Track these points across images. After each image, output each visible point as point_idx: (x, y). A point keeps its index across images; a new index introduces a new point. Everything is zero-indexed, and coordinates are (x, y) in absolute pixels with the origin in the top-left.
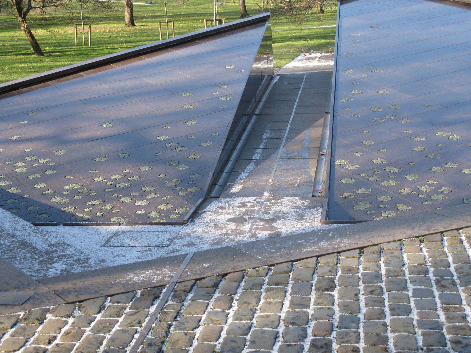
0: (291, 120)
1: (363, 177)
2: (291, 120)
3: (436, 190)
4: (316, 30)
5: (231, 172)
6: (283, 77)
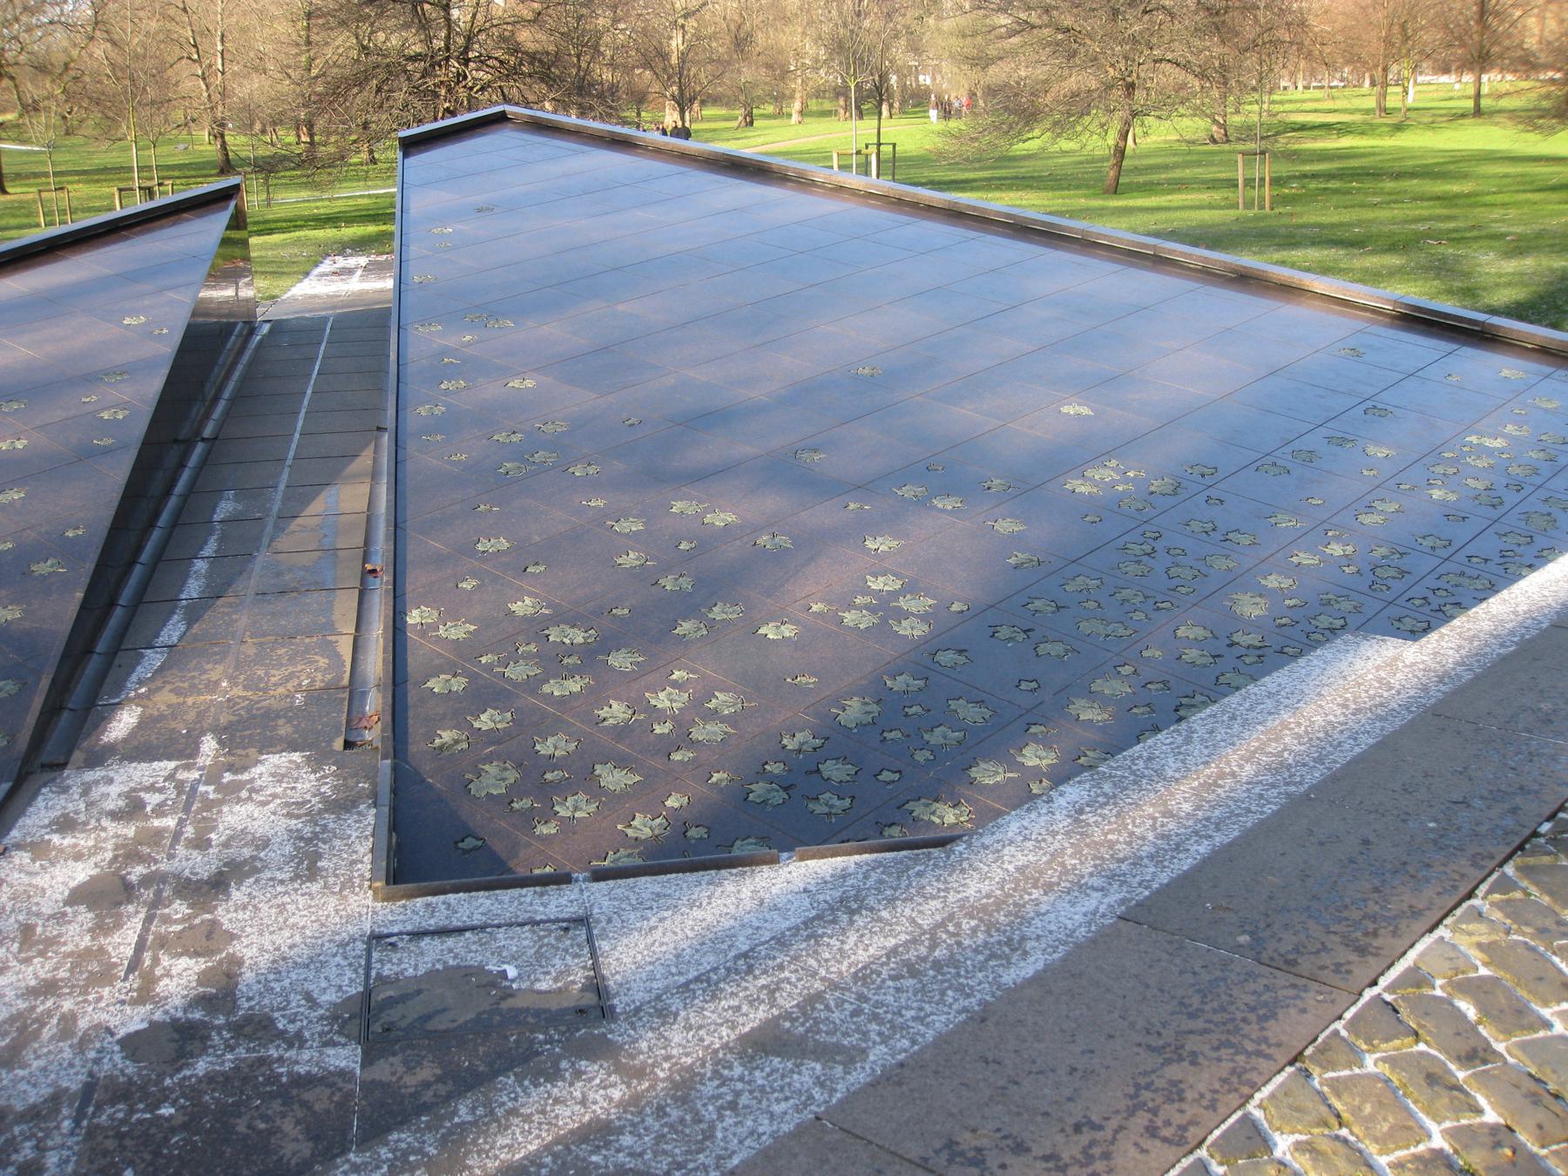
0: (291, 454)
1: (489, 668)
2: (291, 454)
3: (699, 708)
6: (278, 327)
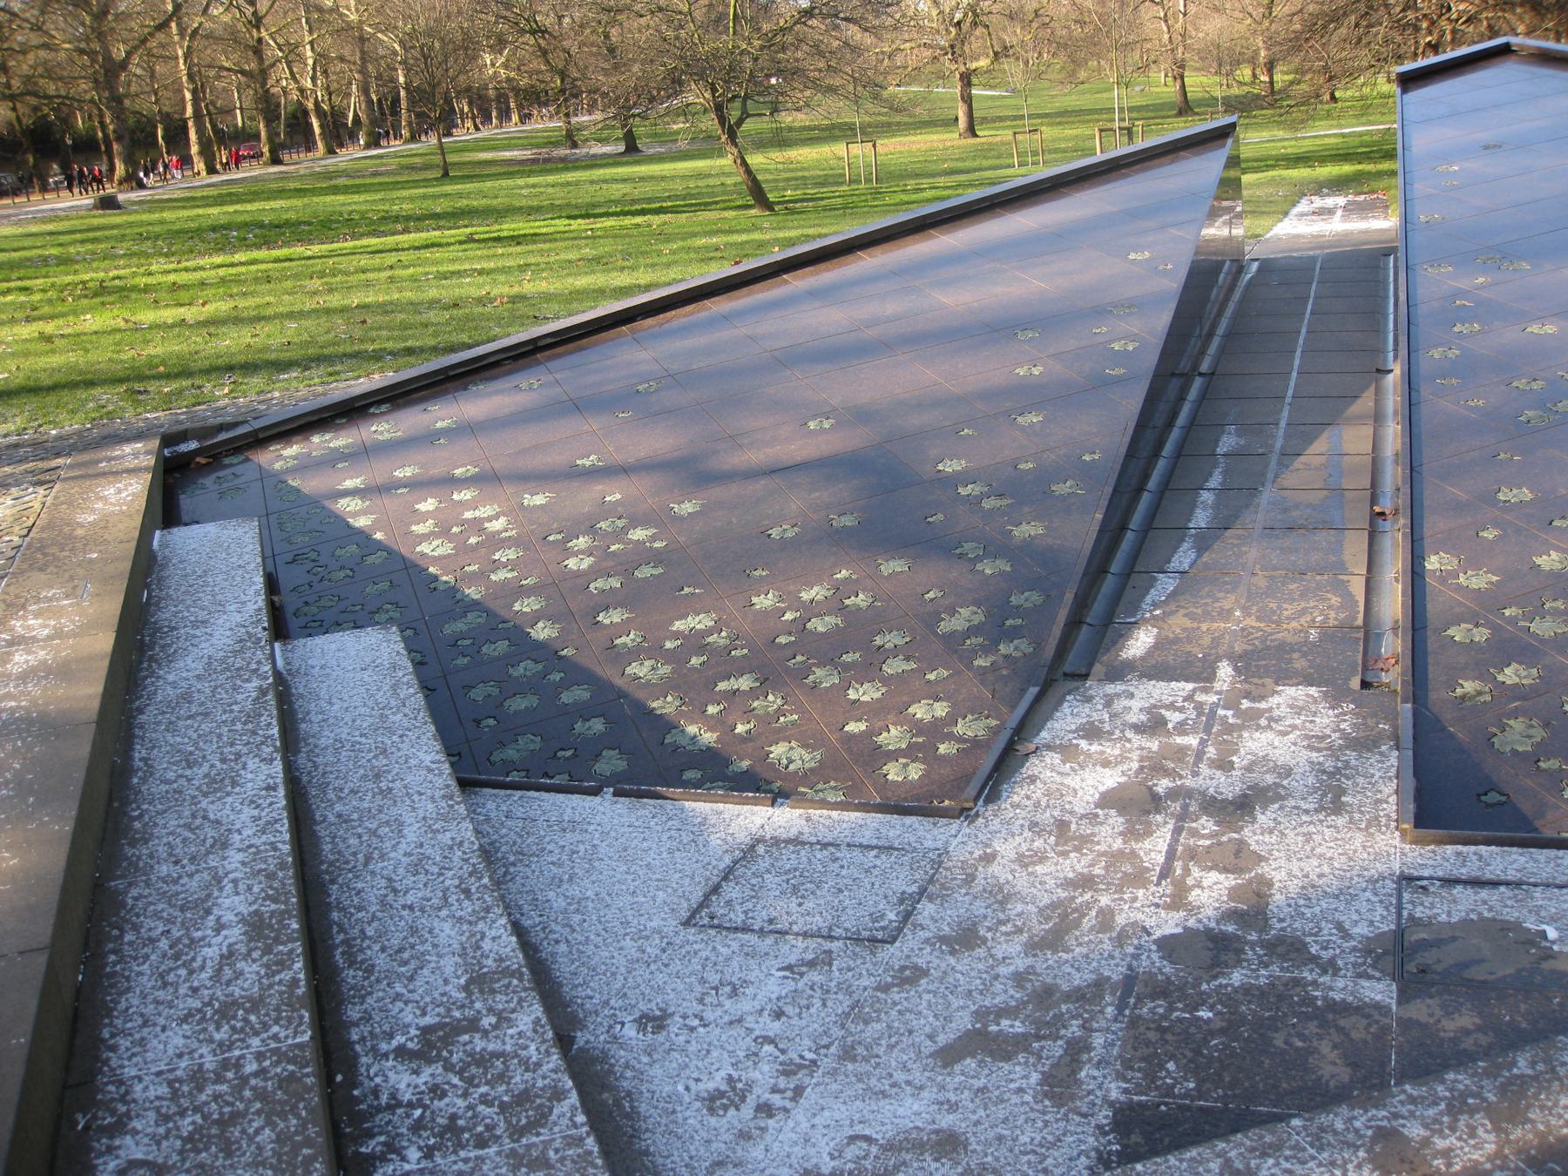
0: (1290, 392)
1: (1513, 621)
2: (1290, 392)
4: (1327, 141)
5: (1129, 575)
6: (1266, 266)
